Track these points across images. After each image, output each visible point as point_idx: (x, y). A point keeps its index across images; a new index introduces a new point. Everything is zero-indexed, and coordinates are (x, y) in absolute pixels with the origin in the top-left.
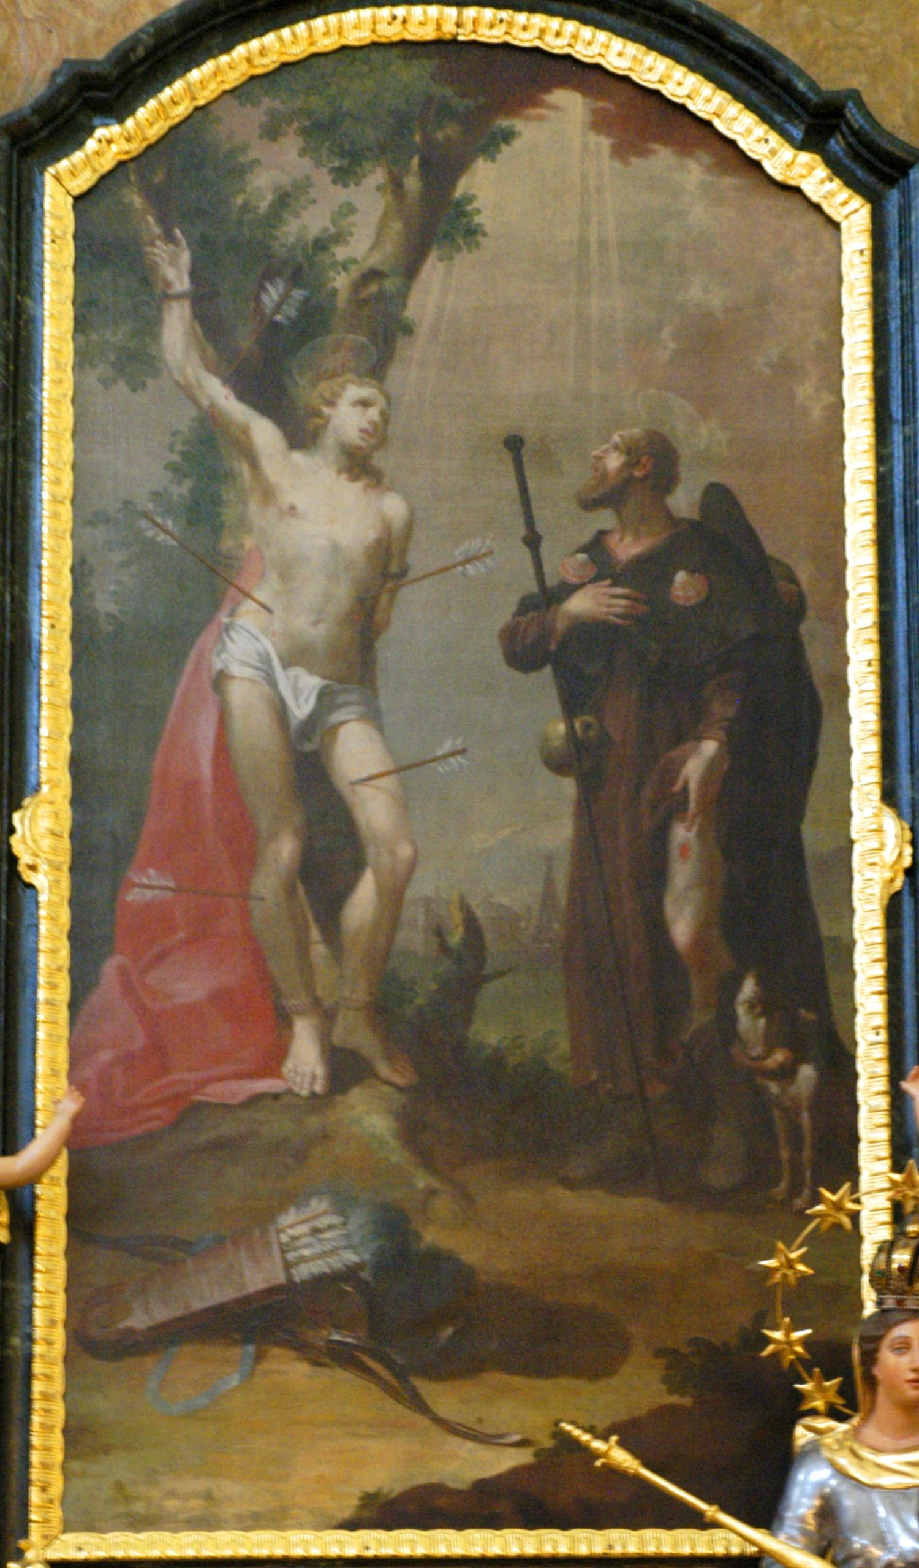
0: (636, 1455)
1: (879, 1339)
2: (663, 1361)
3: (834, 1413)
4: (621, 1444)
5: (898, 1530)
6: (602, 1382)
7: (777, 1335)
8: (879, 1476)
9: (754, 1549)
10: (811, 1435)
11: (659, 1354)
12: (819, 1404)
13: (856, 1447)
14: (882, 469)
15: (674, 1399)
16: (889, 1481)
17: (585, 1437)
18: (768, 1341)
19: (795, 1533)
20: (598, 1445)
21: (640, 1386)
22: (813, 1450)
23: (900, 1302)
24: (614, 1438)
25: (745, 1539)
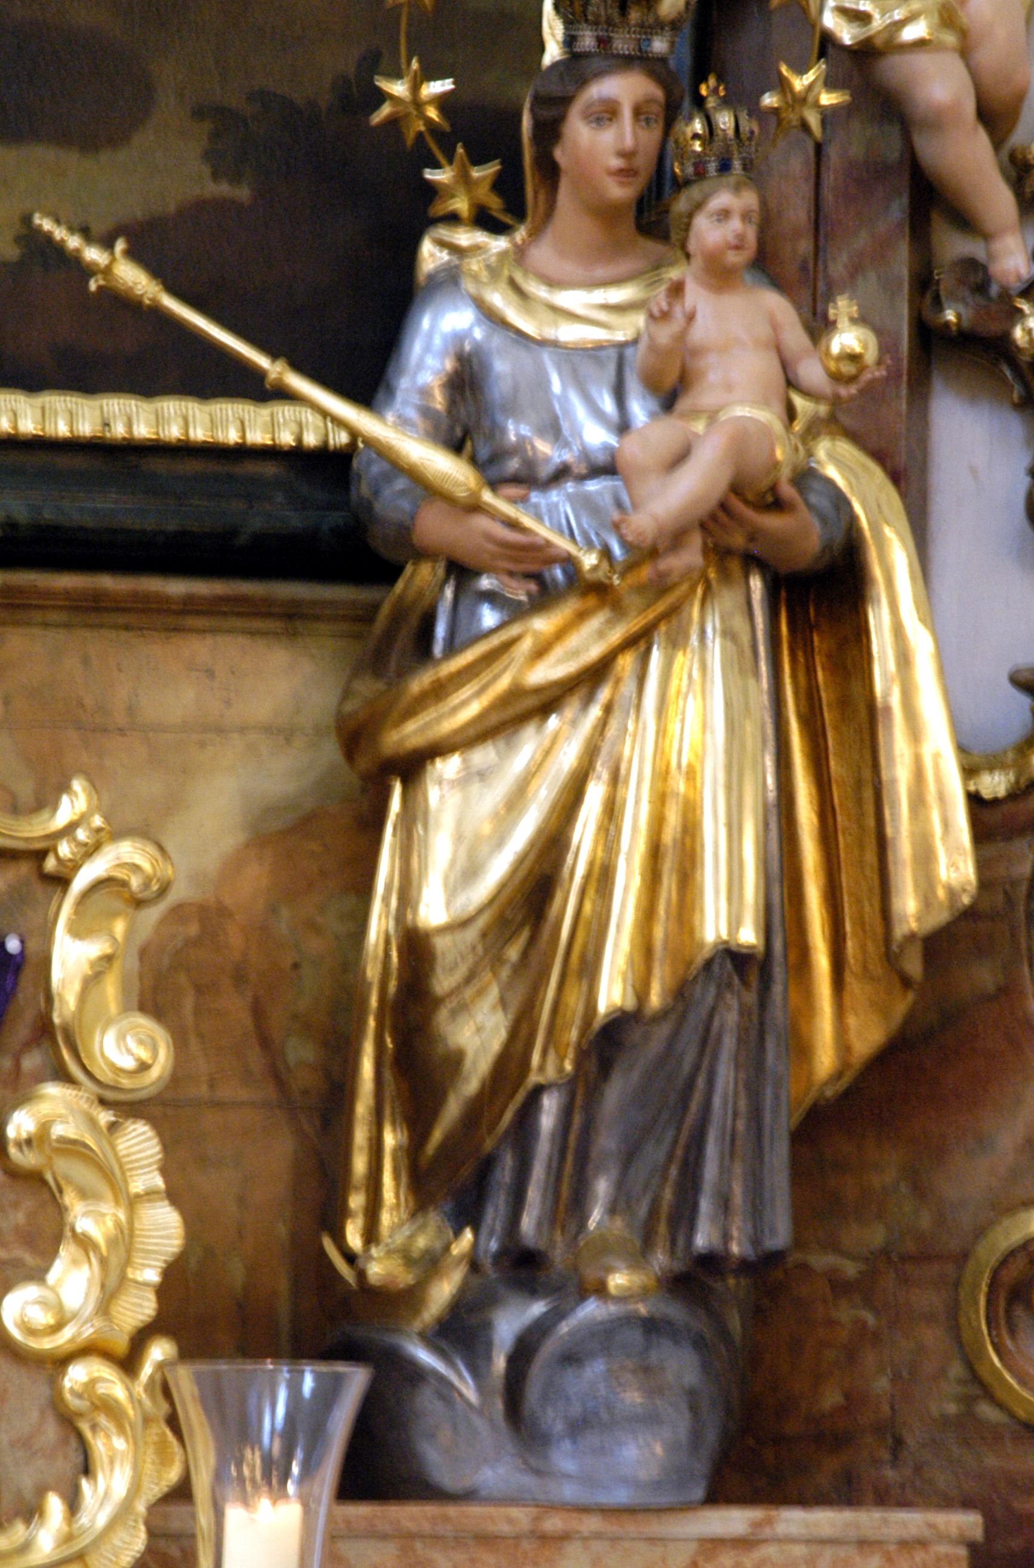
0: (155, 271)
1: (566, 101)
2: (207, 126)
3: (484, 221)
4: (134, 254)
5: (580, 411)
6: (104, 156)
7: (398, 89)
8: (556, 325)
9: (342, 438)
10: (444, 256)
11: (199, 113)
12: (461, 205)
13: (519, 277)
14: (571, 88)
15: (223, 189)
16: (569, 333)
17: (73, 242)
18: (382, 97)
19: (412, 414)
20: (93, 255)
21: (170, 167)
22: (449, 279)
23: (603, 42)
24: (120, 246)
25: (339, 423)
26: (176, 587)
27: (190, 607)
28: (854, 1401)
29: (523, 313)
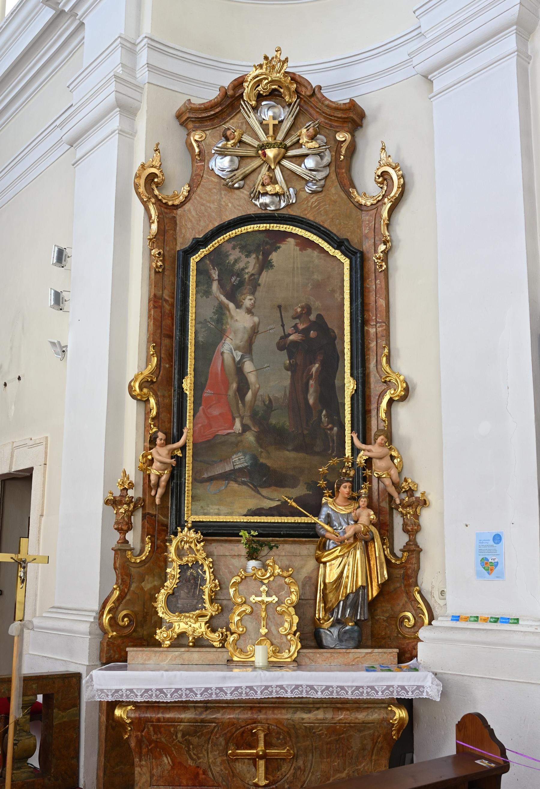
3: (330, 496)
11: (305, 484)
12: (327, 495)
15: (309, 492)
26: (304, 539)
27: (306, 541)
28: (386, 634)
29: (335, 507)
